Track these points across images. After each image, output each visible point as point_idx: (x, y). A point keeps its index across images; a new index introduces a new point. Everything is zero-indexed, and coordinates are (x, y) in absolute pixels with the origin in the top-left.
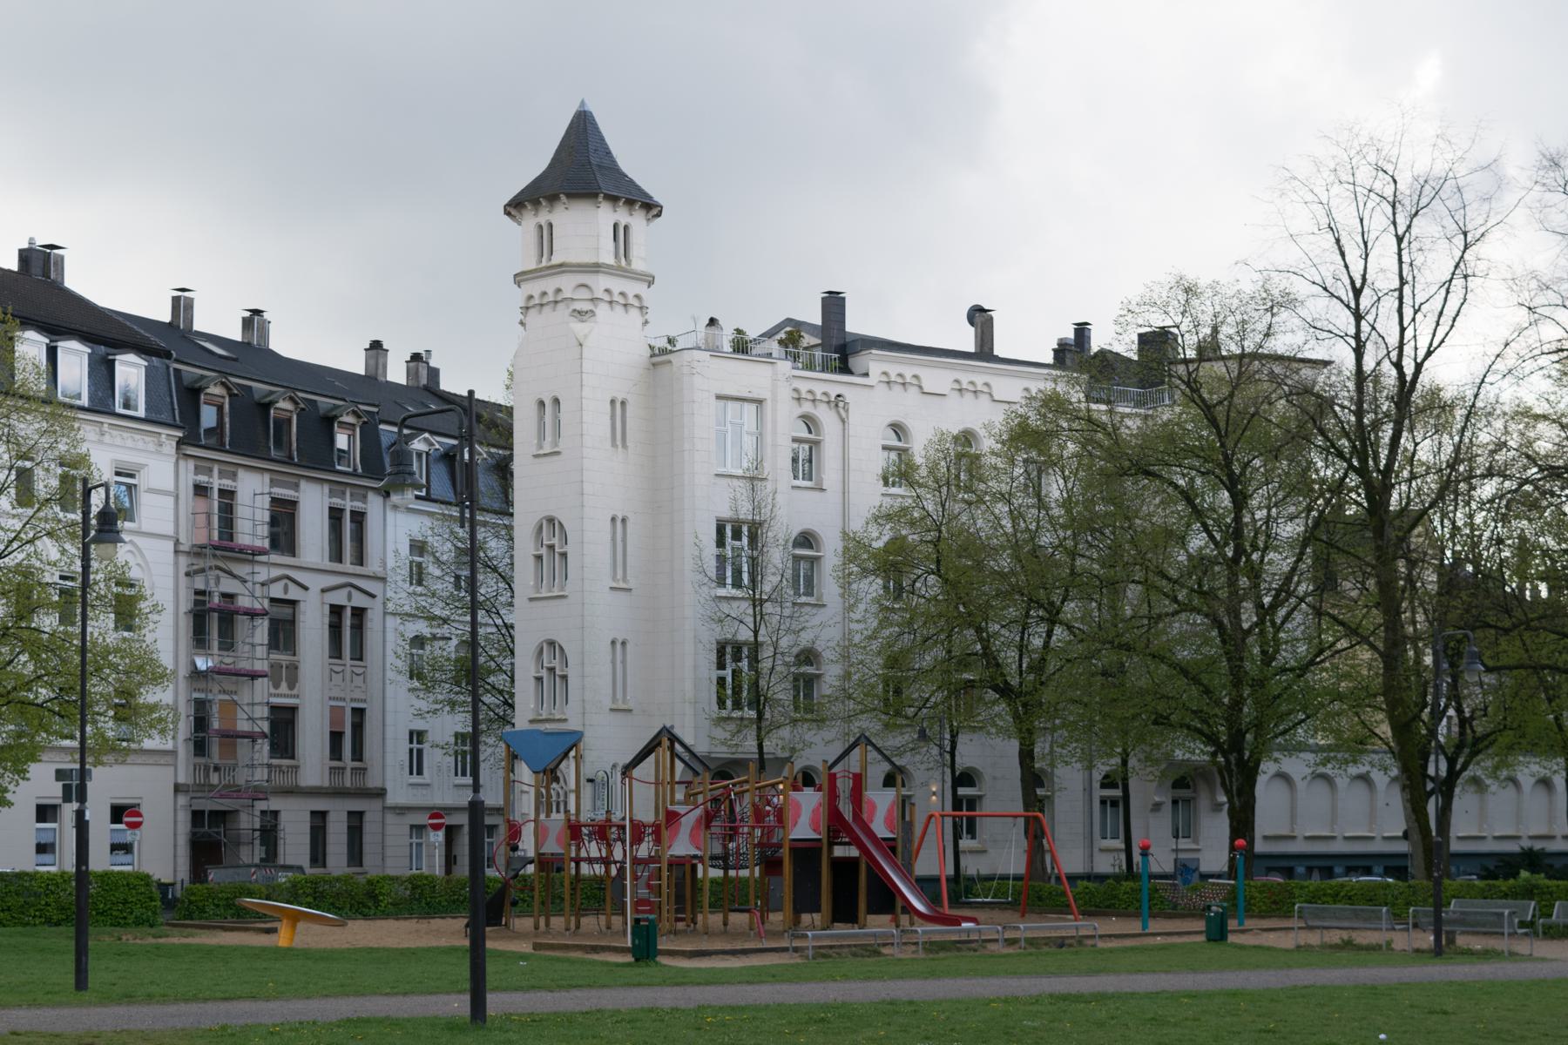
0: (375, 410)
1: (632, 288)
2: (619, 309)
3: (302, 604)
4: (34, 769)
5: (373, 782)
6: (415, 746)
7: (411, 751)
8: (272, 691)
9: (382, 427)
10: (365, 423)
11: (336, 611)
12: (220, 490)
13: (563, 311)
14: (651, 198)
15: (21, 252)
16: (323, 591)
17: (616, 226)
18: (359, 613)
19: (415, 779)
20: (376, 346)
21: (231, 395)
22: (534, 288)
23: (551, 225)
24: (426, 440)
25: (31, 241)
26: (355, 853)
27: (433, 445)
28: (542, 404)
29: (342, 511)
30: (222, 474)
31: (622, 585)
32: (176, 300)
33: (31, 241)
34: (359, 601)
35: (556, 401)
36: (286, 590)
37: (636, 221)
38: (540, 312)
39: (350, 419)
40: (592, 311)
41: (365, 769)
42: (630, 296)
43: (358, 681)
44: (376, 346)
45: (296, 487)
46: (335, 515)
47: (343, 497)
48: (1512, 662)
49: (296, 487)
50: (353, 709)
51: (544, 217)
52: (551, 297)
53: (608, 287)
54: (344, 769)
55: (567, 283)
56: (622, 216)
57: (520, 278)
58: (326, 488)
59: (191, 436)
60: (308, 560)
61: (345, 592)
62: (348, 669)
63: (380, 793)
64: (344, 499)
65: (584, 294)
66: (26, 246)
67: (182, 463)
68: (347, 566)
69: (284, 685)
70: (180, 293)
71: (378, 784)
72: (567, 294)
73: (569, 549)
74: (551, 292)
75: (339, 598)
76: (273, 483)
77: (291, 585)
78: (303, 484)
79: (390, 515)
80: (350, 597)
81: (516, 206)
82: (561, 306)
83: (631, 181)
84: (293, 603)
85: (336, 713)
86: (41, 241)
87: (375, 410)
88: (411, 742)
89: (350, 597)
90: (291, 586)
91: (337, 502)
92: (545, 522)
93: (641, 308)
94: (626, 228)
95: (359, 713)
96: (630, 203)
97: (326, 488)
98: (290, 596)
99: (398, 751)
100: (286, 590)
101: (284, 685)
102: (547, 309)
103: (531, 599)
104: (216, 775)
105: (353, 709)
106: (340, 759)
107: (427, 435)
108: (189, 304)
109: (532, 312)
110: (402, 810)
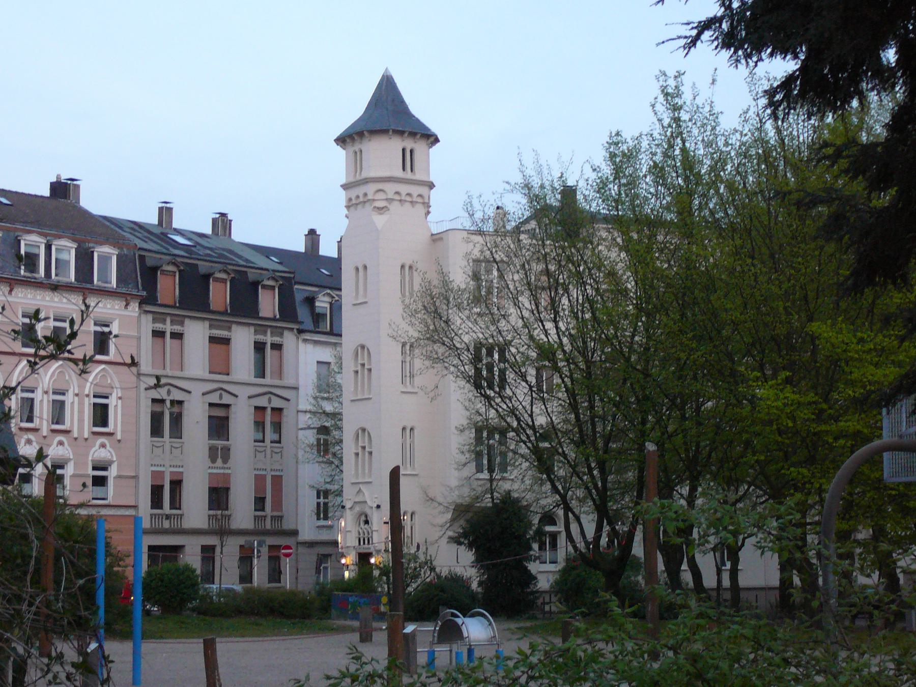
0: (292, 276)
1: (415, 190)
2: (408, 205)
3: (285, 410)
4: (467, 556)
5: (287, 525)
6: (322, 500)
7: (318, 504)
8: (211, 465)
9: (296, 287)
10: (280, 285)
11: (260, 410)
12: (171, 333)
13: (369, 208)
14: (429, 130)
15: (52, 184)
16: (250, 397)
17: (404, 150)
18: (278, 411)
19: (322, 523)
20: (312, 232)
21: (180, 271)
22: (354, 193)
23: (361, 151)
24: (329, 294)
25: (58, 176)
26: (275, 574)
27: (333, 297)
28: (357, 269)
29: (264, 344)
30: (172, 323)
31: (409, 389)
32: (161, 209)
33: (58, 176)
34: (276, 403)
35: (365, 267)
36: (221, 397)
37: (419, 147)
38: (363, 207)
39: (271, 283)
40: (386, 207)
41: (282, 517)
42: (415, 195)
43: (177, 452)
44: (312, 232)
45: (229, 329)
46: (259, 347)
47: (265, 333)
48: (534, 410)
49: (229, 329)
50: (272, 476)
51: (357, 147)
52: (361, 199)
53: (397, 190)
54: (265, 517)
55: (371, 189)
56: (409, 144)
57: (345, 187)
58: (252, 329)
59: (149, 299)
60: (286, 381)
61: (267, 397)
62: (268, 452)
63: (295, 533)
64: (266, 336)
65: (381, 196)
66: (55, 180)
67: (143, 317)
68: (268, 380)
69: (219, 460)
70: (164, 205)
71: (292, 527)
72: (370, 197)
73: (373, 367)
74: (361, 195)
75: (262, 402)
76: (211, 327)
77: (224, 394)
78: (234, 327)
79: (302, 346)
80: (270, 401)
81: (342, 140)
82: (367, 205)
83: (418, 120)
84: (227, 406)
85: (259, 480)
86: (64, 177)
87: (292, 276)
88: (318, 497)
89: (270, 401)
90: (224, 394)
91: (260, 338)
92: (359, 348)
93: (424, 203)
94: (412, 151)
95: (277, 481)
96: (413, 134)
97: (252, 329)
98: (224, 402)
99: (308, 502)
100: (221, 397)
101: (219, 460)
102: (359, 207)
103: (352, 401)
104: (168, 521)
105: (272, 476)
106: (263, 509)
107: (329, 291)
108: (170, 210)
109: (352, 209)
110: (311, 544)
